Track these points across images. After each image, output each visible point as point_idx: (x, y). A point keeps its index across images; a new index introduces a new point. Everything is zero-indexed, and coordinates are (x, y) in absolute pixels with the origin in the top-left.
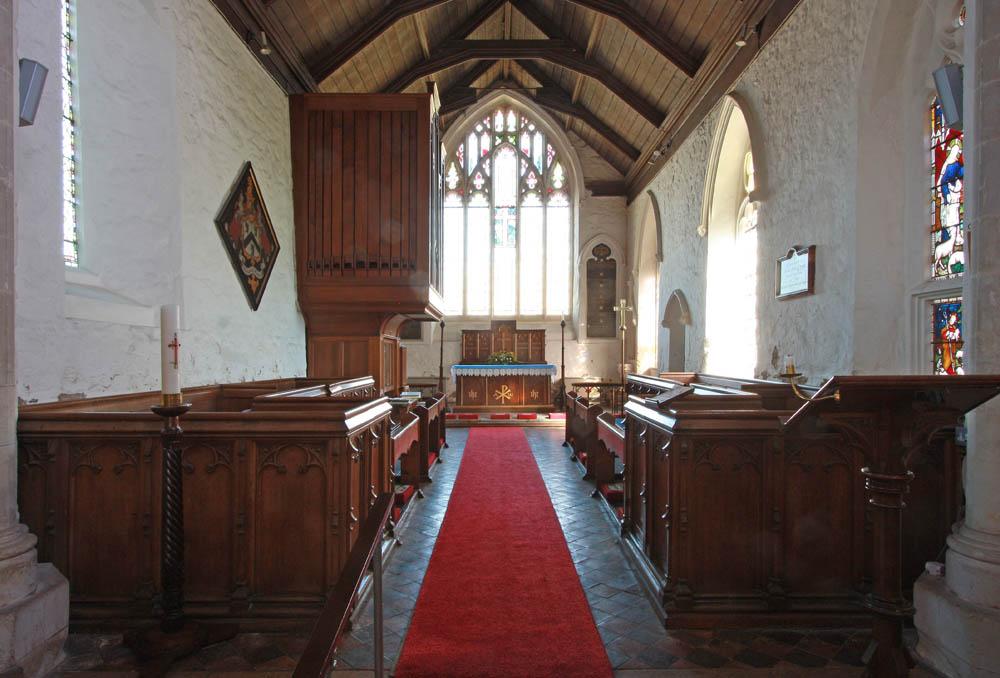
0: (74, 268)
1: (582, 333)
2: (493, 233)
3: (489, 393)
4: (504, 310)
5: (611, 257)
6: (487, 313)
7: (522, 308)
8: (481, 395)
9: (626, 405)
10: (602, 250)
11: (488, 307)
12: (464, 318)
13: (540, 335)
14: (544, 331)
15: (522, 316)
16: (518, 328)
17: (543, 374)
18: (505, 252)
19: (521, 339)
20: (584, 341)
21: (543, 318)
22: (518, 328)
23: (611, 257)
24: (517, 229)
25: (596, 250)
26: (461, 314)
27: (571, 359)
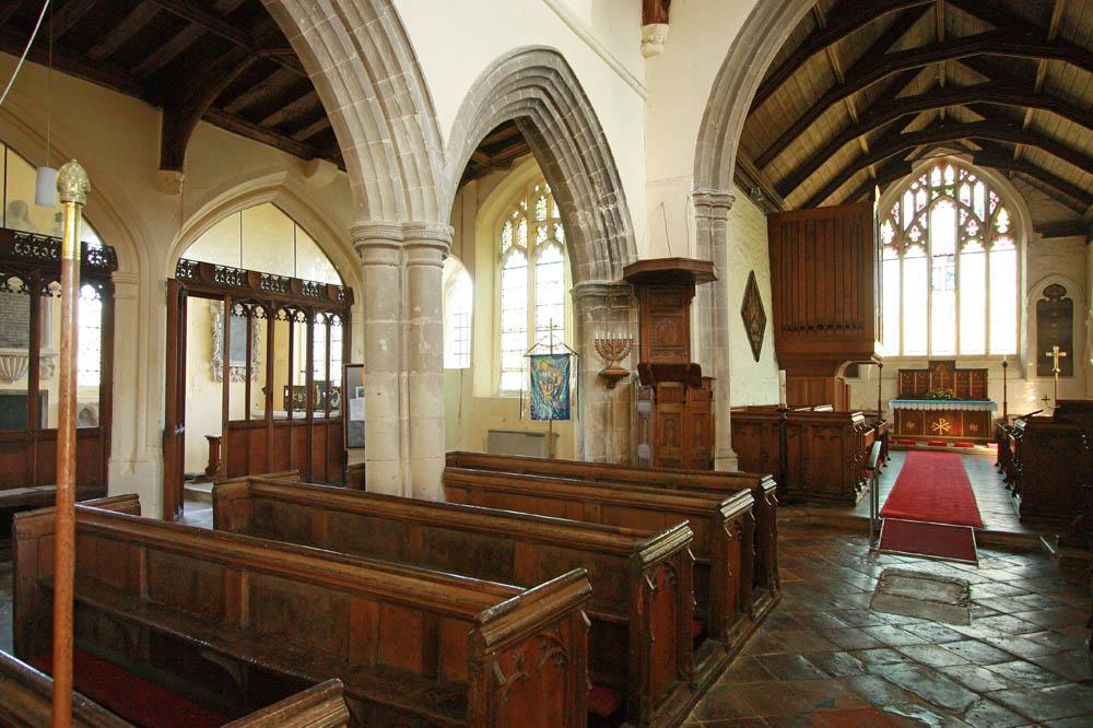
4: (943, 349)
5: (1043, 297)
10: (1054, 291)
13: (982, 375)
15: (963, 356)
22: (957, 367)
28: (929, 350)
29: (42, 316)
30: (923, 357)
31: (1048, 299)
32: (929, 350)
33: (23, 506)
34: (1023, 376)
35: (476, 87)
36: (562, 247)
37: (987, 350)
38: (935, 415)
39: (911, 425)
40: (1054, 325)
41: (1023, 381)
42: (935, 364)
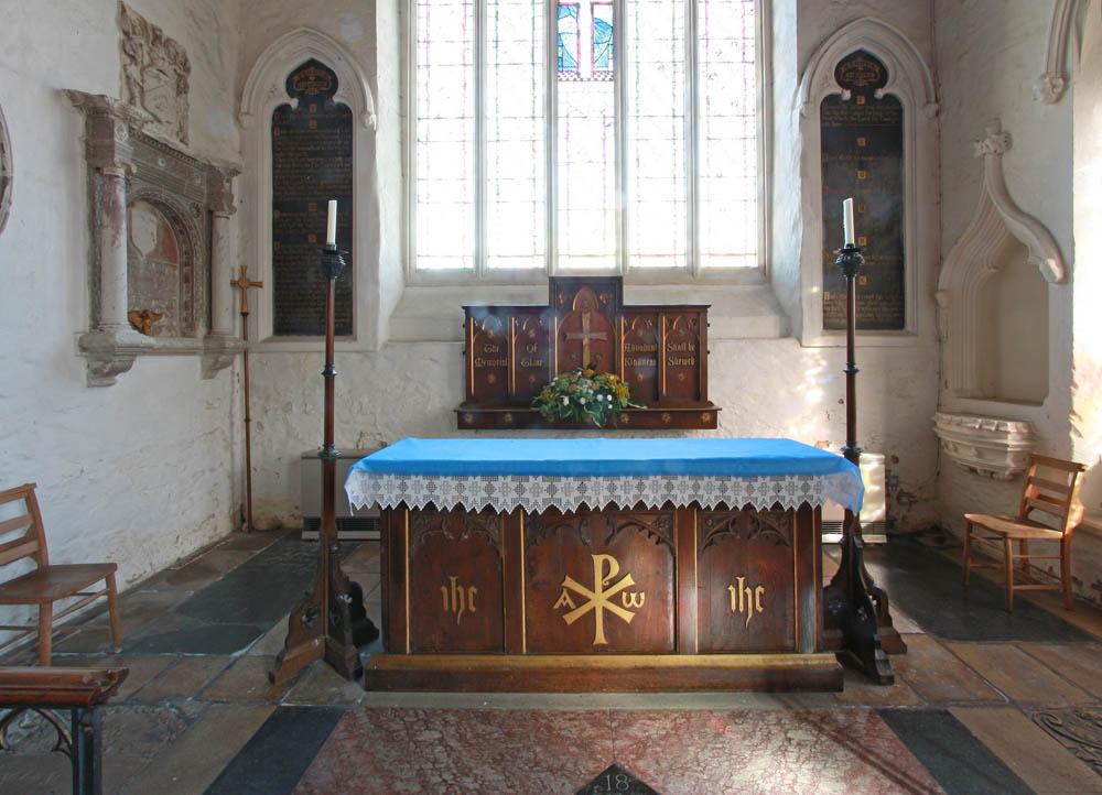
0: (644, 411)
1: (812, 317)
2: (553, 39)
3: (533, 587)
4: (586, 254)
5: (837, 89)
6: (540, 263)
7: (704, 244)
8: (499, 596)
9: (841, 536)
10: (860, 72)
11: (542, 247)
12: (476, 277)
13: (692, 320)
14: (705, 308)
15: (634, 271)
16: (627, 302)
17: (791, 501)
18: (585, 98)
19: (609, 349)
20: (819, 341)
21: (690, 275)
22: (627, 302)
23: (837, 89)
24: (618, 28)
25: (844, 72)
26: (470, 264)
27: (782, 393)
28: (551, 254)
29: (872, 331)
30: (534, 272)
31: (847, 95)
32: (551, 254)
33: (826, 221)
34: (790, 330)
35: (572, 437)
36: (152, 122)
37: (694, 251)
38: (505, 413)
39: (459, 597)
40: (862, 175)
41: (789, 343)
42: (567, 288)
